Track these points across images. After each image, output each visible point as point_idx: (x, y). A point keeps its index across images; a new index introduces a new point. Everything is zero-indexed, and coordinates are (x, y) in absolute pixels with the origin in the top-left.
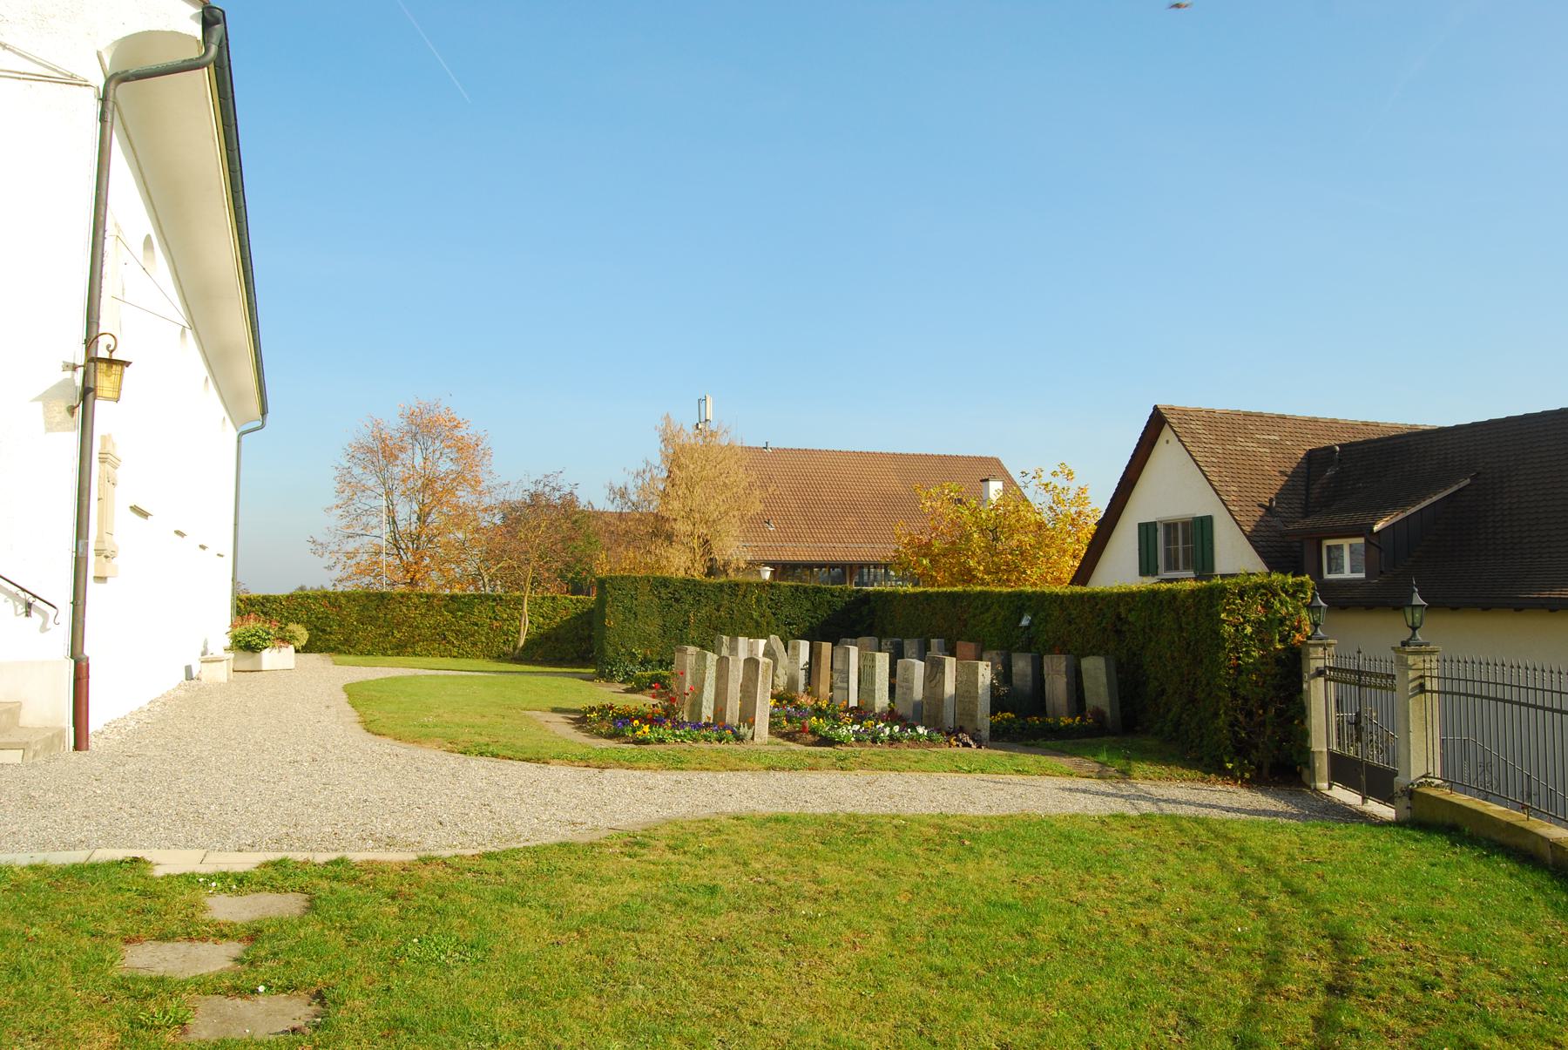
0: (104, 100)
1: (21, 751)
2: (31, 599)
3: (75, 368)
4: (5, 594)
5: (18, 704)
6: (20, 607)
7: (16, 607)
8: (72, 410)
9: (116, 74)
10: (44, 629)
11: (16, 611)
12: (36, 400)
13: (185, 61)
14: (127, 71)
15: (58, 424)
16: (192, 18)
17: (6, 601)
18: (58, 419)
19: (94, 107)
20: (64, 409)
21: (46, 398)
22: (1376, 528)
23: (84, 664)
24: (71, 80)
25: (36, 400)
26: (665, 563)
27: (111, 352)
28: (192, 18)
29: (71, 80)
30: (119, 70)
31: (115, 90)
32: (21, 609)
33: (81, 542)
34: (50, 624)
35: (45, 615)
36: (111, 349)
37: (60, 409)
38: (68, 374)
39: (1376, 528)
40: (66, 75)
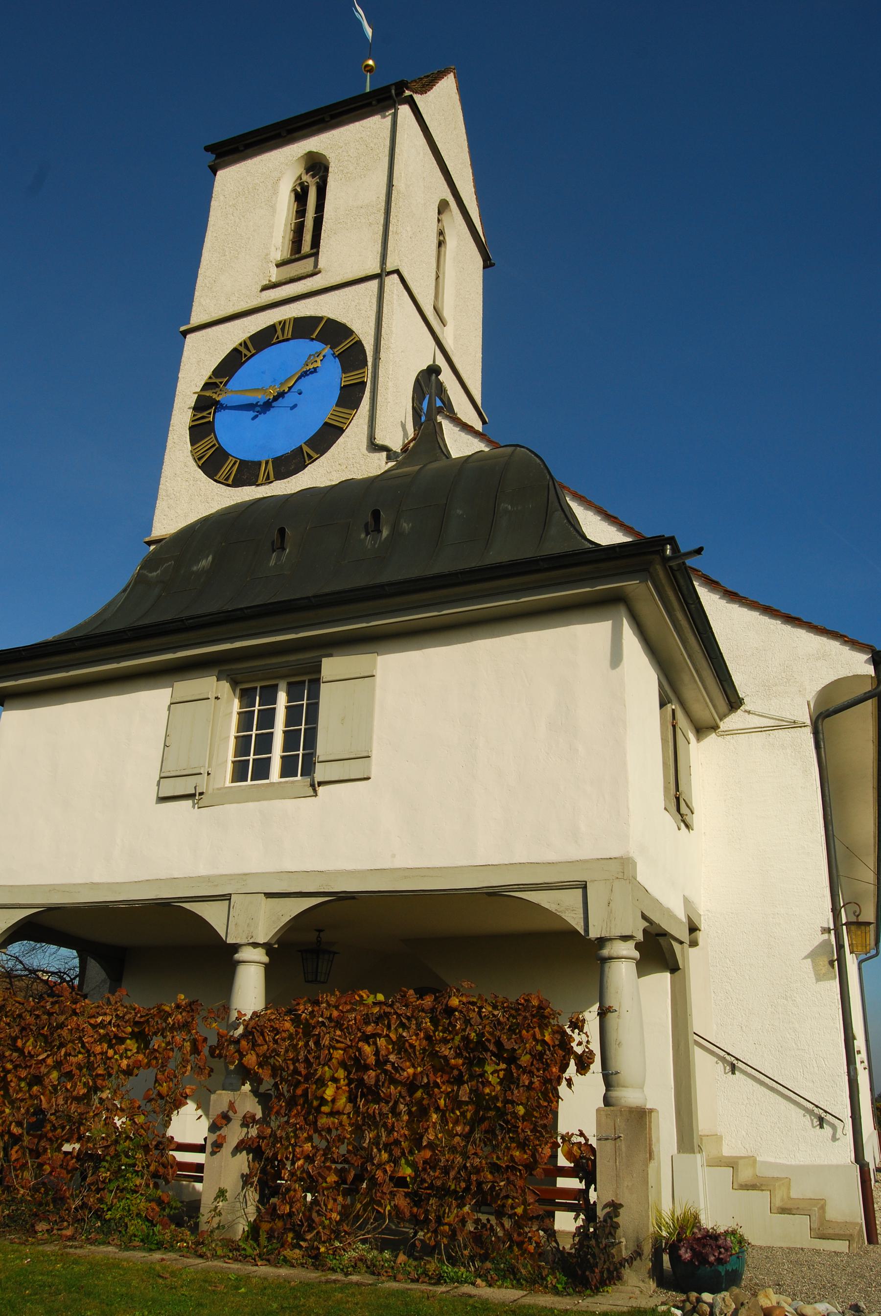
0: (816, 733)
1: (847, 1242)
2: (823, 1115)
3: (828, 930)
4: (804, 1110)
5: (822, 1202)
6: (815, 1120)
7: (812, 1121)
8: (831, 963)
9: (821, 713)
10: (834, 1138)
11: (812, 1124)
12: (806, 958)
13: (865, 693)
14: (828, 710)
15: (824, 974)
16: (866, 662)
17: (804, 1116)
18: (823, 971)
19: (810, 737)
20: (826, 963)
21: (813, 955)
22: (668, 547)
23: (866, 1169)
24: (795, 725)
25: (806, 958)
26: (69, 1232)
27: (858, 916)
28: (866, 662)
29: (795, 725)
30: (823, 709)
31: (822, 725)
32: (816, 1122)
33: (851, 1068)
34: (839, 1134)
35: (834, 1127)
36: (857, 914)
37: (824, 962)
38: (826, 936)
39: (668, 547)
40: (791, 722)
